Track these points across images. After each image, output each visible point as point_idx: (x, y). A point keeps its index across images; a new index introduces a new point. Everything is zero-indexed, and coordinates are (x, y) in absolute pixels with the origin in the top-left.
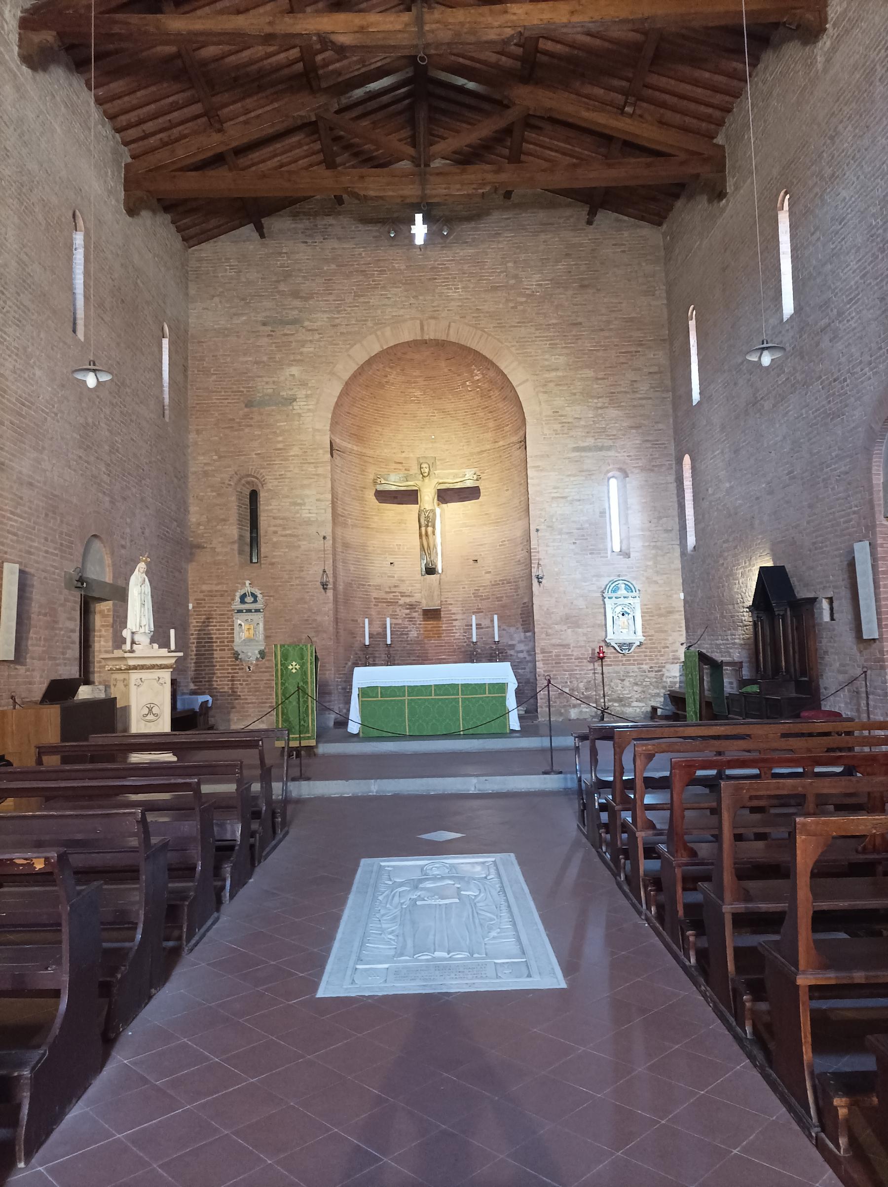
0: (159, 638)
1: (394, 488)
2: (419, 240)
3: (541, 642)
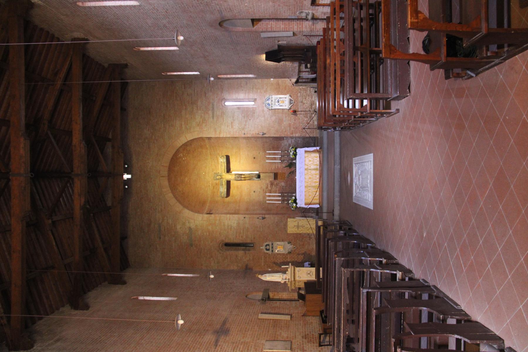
0: (284, 272)
1: (226, 190)
2: (129, 176)
3: (289, 134)
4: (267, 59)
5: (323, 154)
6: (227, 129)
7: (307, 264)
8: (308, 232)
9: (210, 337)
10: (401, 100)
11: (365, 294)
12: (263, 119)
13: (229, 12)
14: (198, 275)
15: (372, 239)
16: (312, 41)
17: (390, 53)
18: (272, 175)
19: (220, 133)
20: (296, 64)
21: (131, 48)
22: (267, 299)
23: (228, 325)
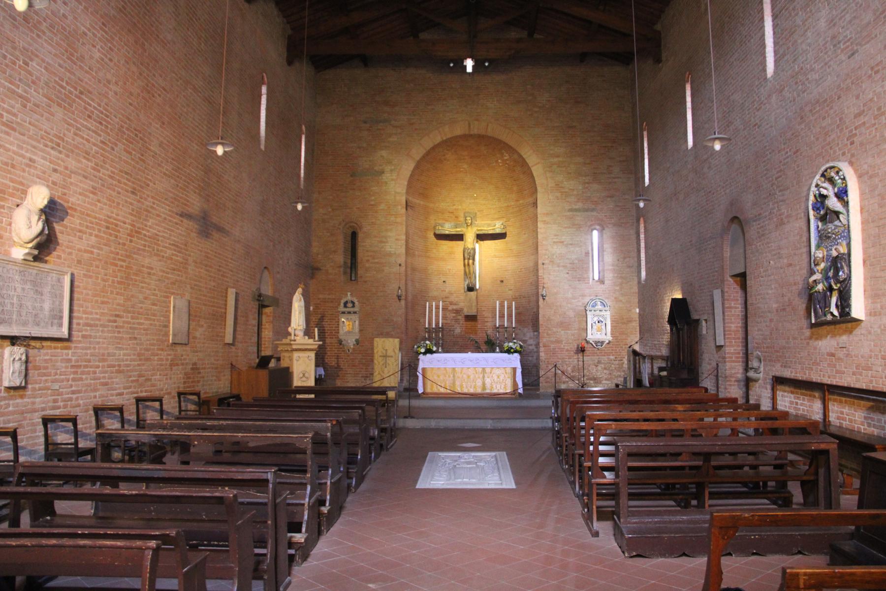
0: (308, 333)
1: (447, 232)
2: (469, 69)
3: (544, 340)
4: (674, 301)
5: (511, 399)
6: (552, 234)
7: (321, 371)
8: (375, 374)
9: (196, 204)
10: (616, 539)
11: (264, 476)
12: (570, 295)
13: (758, 232)
14: (302, 187)
15: (363, 487)
16: (707, 380)
17: (721, 528)
18: (473, 312)
19: (545, 222)
20: (665, 352)
21: (693, 69)
22: (262, 303)
23: (216, 235)
